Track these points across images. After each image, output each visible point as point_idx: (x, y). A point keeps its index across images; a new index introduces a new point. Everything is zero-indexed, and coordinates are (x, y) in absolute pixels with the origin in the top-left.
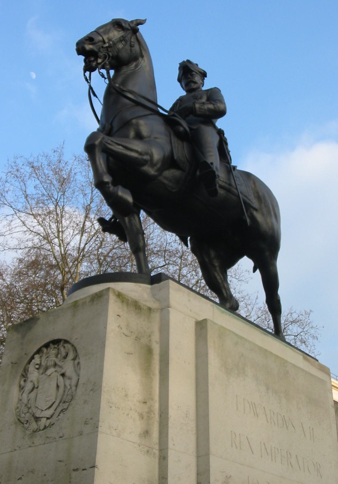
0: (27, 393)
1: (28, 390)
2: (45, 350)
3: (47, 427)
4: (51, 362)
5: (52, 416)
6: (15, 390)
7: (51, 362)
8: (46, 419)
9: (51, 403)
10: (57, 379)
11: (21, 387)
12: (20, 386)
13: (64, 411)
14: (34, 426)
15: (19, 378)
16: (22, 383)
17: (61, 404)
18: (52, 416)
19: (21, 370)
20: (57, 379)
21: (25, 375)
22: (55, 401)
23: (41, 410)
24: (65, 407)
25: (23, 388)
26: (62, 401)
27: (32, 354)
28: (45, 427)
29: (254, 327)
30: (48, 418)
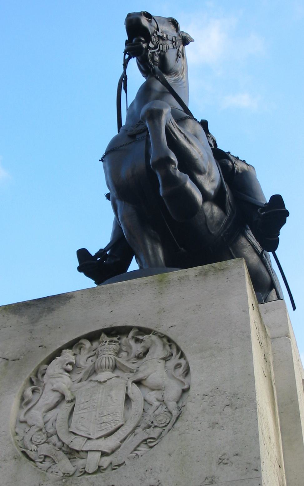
0: (44, 409)
1: (47, 404)
2: (87, 344)
3: (104, 470)
4: (109, 361)
5: (113, 452)
6: (13, 402)
7: (109, 361)
8: (100, 454)
9: (115, 427)
10: (127, 387)
11: (26, 400)
12: (22, 399)
13: (150, 442)
14: (66, 465)
15: (23, 382)
16: (29, 392)
17: (138, 430)
18: (113, 452)
19: (29, 372)
20: (127, 387)
21: (35, 381)
22: (122, 425)
23: (86, 439)
24: (155, 435)
25: (27, 403)
26: (143, 425)
27: (59, 346)
28: (99, 469)
29: (254, 297)
30: (104, 454)
